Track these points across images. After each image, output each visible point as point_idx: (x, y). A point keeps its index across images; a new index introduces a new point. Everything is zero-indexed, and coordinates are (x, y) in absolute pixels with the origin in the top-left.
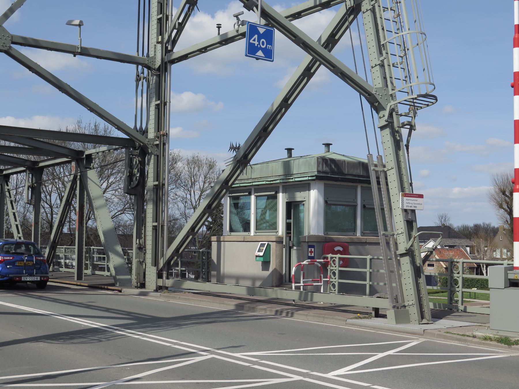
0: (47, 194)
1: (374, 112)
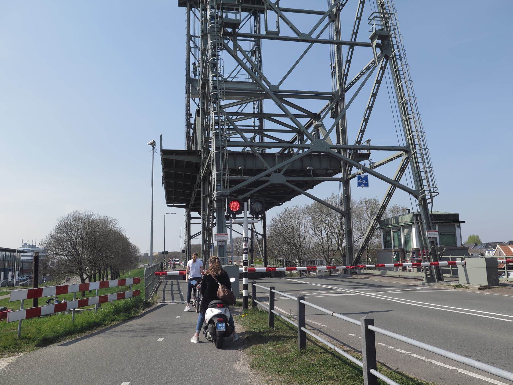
0: (319, 231)
1: (416, 199)
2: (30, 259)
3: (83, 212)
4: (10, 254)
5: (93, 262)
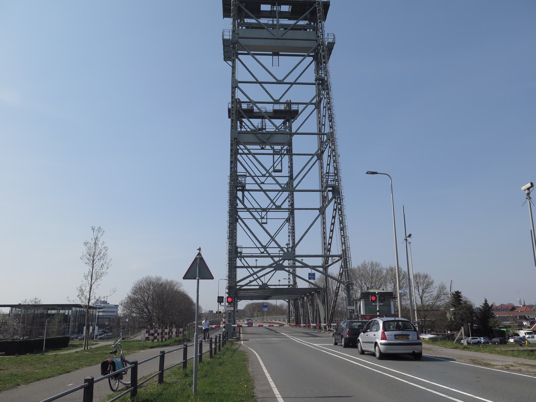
2: (102, 315)
3: (154, 276)
4: (80, 310)
5: (161, 319)
